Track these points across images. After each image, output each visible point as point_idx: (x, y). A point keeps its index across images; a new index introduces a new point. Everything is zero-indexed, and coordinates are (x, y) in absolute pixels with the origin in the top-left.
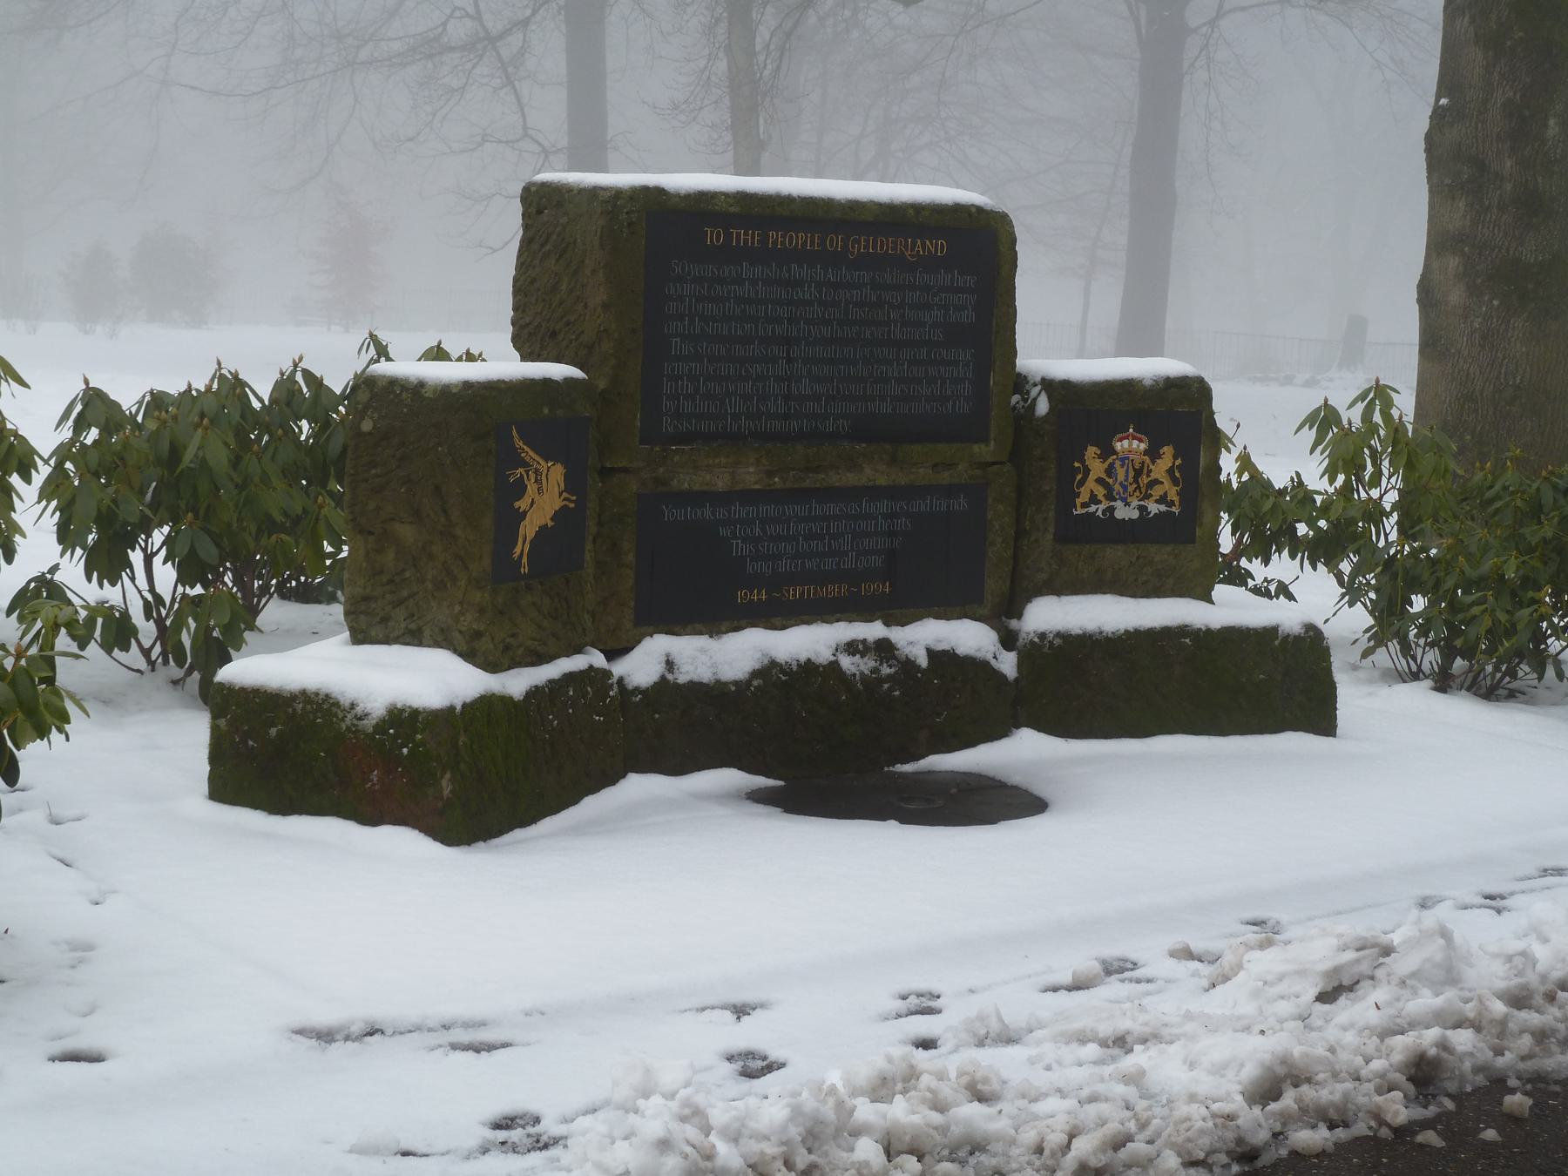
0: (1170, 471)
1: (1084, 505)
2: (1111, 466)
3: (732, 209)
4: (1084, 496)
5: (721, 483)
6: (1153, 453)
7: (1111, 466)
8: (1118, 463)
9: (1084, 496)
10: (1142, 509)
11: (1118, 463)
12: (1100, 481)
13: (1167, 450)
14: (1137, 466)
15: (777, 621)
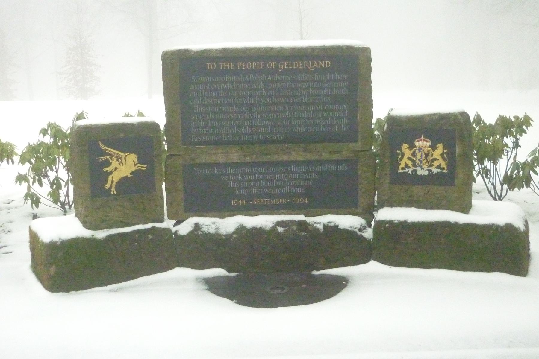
0: (442, 155)
1: (403, 169)
2: (414, 152)
3: (219, 55)
4: (402, 165)
5: (221, 159)
6: (433, 147)
7: (414, 152)
8: (417, 151)
9: (402, 165)
10: (429, 171)
11: (417, 151)
12: (409, 158)
13: (440, 146)
14: (426, 153)
15: (252, 212)
